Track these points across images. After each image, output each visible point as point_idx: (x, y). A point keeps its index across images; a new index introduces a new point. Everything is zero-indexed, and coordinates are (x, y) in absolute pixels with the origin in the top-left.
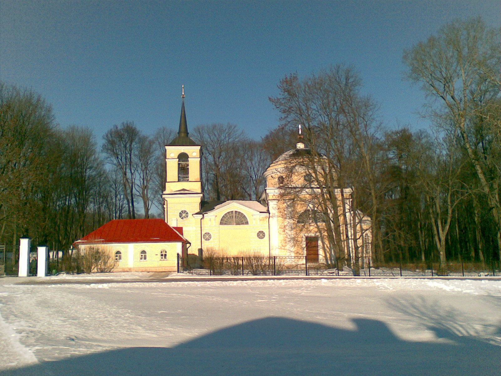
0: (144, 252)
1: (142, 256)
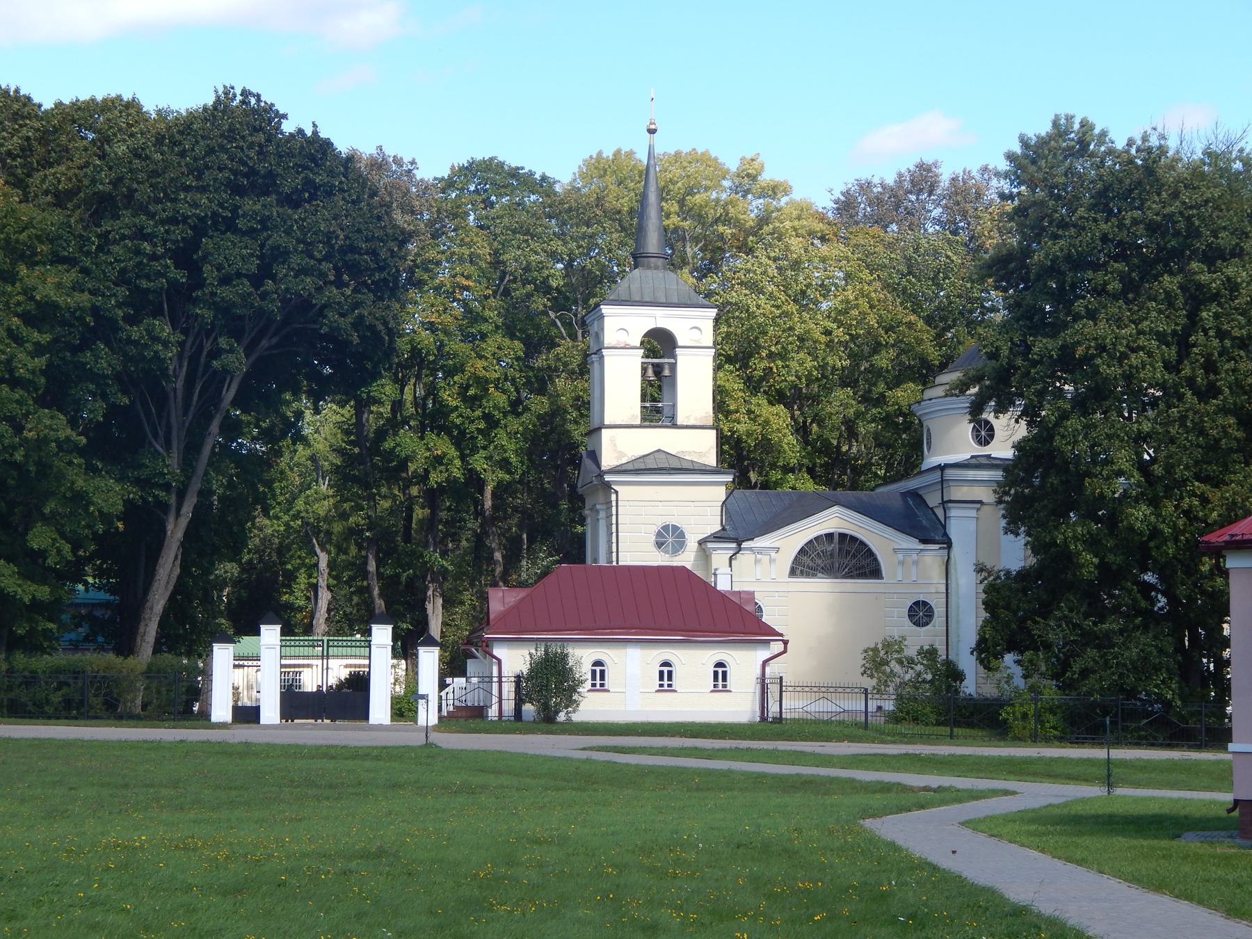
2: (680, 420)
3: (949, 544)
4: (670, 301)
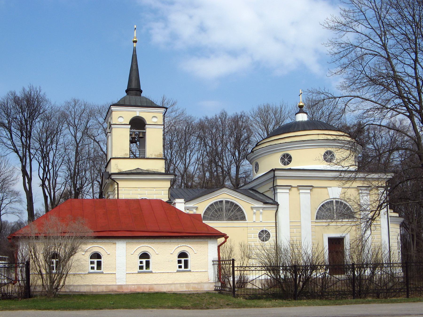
0: (97, 256)
1: (141, 262)
2: (148, 155)
3: (278, 205)
4: (143, 105)
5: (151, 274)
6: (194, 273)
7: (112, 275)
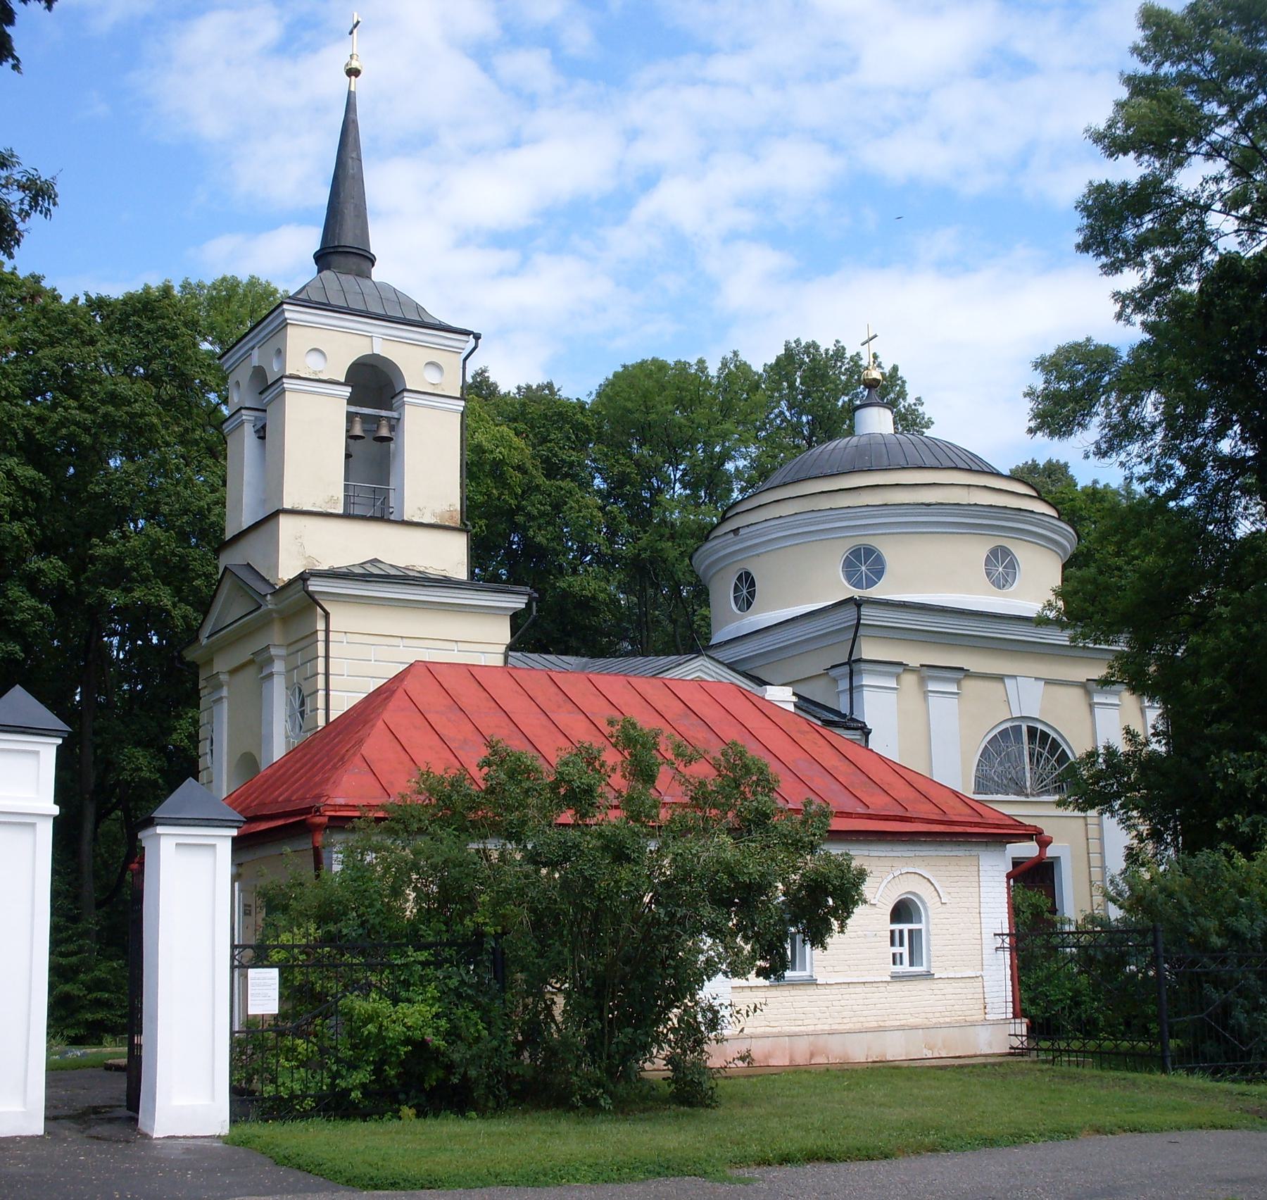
5: (811, 991)
6: (940, 984)
7: (851, 990)
